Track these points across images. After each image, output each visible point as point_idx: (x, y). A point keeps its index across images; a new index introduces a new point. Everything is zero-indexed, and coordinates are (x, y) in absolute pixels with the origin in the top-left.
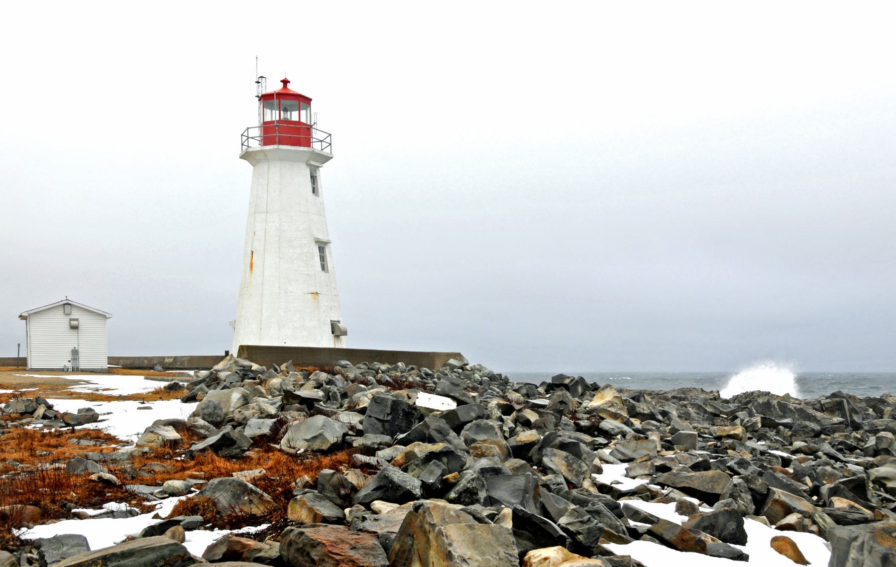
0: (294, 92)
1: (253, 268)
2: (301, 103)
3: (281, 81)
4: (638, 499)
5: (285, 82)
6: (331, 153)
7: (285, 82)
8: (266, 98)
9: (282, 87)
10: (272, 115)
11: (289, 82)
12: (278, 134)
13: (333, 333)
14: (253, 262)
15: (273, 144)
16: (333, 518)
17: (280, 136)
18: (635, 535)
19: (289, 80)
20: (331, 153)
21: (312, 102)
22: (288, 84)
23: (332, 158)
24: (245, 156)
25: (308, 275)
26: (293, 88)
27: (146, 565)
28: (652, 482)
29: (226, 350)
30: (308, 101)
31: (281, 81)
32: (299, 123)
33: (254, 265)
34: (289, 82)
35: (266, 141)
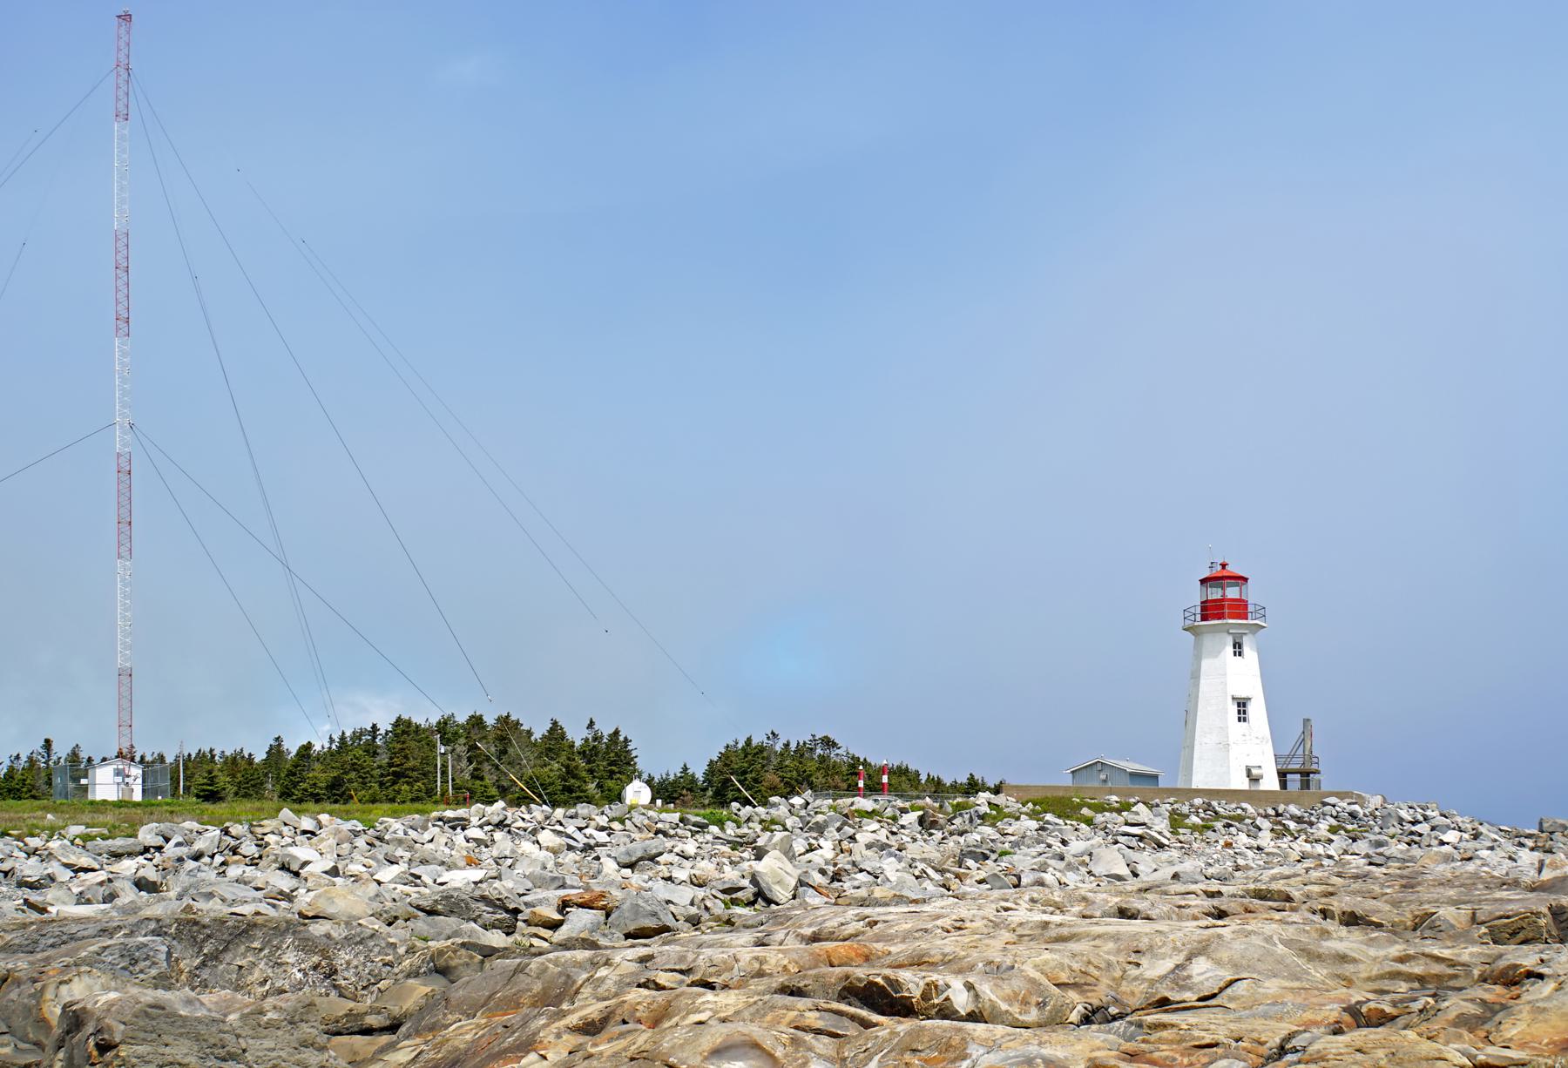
0: (1232, 572)
5: (1224, 566)
7: (1224, 566)
13: (1248, 776)
19: (1227, 561)
25: (1221, 728)
30: (1246, 580)
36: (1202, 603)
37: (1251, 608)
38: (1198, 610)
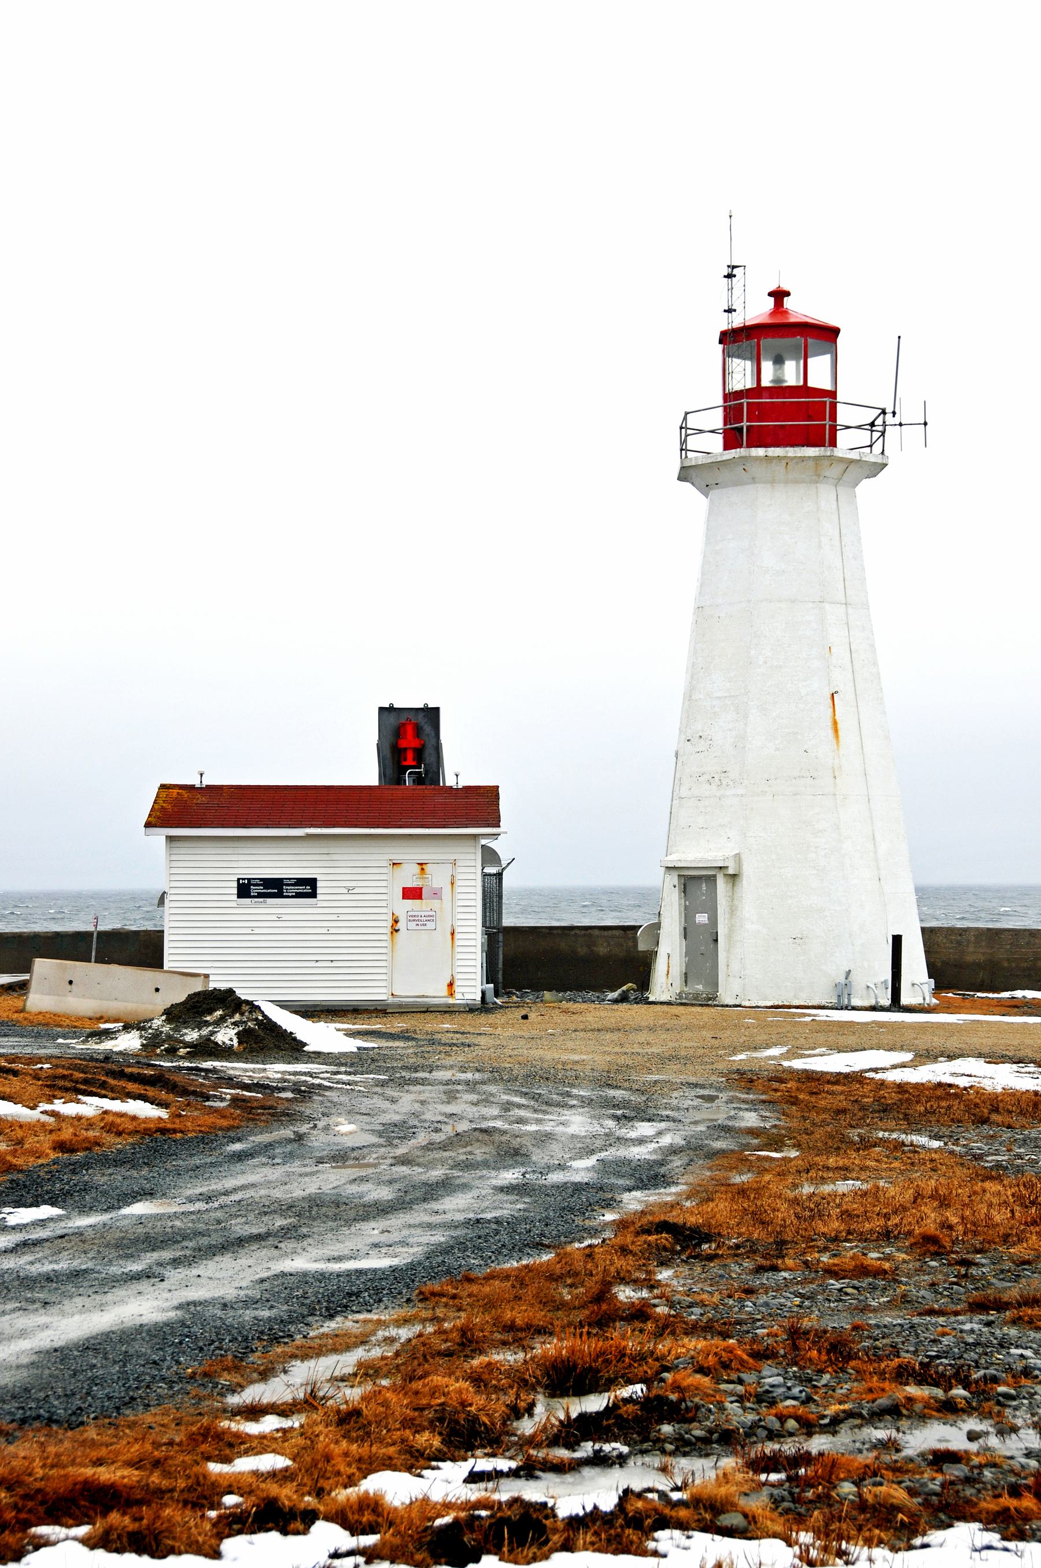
1: (840, 733)
2: (810, 341)
3: (770, 294)
4: (5, 1115)
5: (779, 295)
6: (883, 453)
7: (779, 295)
8: (731, 339)
9: (772, 306)
10: (742, 376)
11: (788, 294)
12: (745, 424)
14: (837, 717)
15: (735, 448)
16: (249, 1303)
17: (751, 426)
18: (86, 1165)
19: (785, 287)
20: (883, 453)
21: (840, 340)
22: (785, 299)
23: (886, 465)
24: (685, 474)
26: (798, 308)
27: (794, 1567)
28: (973, 996)
29: (895, 934)
30: (828, 334)
31: (770, 294)
32: (805, 390)
33: (839, 726)
34: (788, 294)
35: (732, 440)
36: (727, 397)
37: (844, 415)
38: (717, 419)
